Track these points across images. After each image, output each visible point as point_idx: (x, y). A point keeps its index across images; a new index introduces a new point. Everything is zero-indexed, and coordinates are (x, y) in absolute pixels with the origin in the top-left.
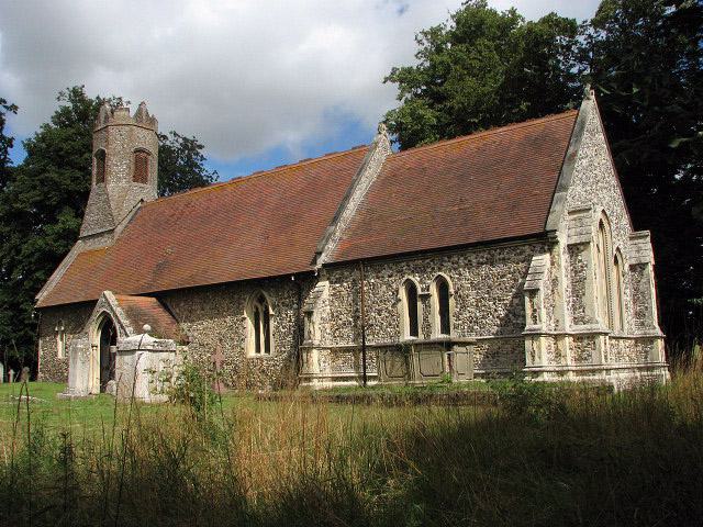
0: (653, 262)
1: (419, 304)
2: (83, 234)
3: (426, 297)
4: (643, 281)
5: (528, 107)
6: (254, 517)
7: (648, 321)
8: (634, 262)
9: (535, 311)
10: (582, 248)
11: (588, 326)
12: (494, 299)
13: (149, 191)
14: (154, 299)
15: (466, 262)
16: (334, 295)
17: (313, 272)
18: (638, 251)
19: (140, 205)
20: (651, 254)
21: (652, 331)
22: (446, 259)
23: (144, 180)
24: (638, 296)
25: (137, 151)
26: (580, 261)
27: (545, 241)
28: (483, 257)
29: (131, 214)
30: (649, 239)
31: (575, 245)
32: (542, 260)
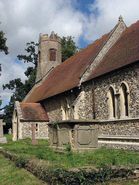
3: (118, 95)
15: (134, 73)
22: (126, 73)
23: (54, 60)
25: (50, 50)
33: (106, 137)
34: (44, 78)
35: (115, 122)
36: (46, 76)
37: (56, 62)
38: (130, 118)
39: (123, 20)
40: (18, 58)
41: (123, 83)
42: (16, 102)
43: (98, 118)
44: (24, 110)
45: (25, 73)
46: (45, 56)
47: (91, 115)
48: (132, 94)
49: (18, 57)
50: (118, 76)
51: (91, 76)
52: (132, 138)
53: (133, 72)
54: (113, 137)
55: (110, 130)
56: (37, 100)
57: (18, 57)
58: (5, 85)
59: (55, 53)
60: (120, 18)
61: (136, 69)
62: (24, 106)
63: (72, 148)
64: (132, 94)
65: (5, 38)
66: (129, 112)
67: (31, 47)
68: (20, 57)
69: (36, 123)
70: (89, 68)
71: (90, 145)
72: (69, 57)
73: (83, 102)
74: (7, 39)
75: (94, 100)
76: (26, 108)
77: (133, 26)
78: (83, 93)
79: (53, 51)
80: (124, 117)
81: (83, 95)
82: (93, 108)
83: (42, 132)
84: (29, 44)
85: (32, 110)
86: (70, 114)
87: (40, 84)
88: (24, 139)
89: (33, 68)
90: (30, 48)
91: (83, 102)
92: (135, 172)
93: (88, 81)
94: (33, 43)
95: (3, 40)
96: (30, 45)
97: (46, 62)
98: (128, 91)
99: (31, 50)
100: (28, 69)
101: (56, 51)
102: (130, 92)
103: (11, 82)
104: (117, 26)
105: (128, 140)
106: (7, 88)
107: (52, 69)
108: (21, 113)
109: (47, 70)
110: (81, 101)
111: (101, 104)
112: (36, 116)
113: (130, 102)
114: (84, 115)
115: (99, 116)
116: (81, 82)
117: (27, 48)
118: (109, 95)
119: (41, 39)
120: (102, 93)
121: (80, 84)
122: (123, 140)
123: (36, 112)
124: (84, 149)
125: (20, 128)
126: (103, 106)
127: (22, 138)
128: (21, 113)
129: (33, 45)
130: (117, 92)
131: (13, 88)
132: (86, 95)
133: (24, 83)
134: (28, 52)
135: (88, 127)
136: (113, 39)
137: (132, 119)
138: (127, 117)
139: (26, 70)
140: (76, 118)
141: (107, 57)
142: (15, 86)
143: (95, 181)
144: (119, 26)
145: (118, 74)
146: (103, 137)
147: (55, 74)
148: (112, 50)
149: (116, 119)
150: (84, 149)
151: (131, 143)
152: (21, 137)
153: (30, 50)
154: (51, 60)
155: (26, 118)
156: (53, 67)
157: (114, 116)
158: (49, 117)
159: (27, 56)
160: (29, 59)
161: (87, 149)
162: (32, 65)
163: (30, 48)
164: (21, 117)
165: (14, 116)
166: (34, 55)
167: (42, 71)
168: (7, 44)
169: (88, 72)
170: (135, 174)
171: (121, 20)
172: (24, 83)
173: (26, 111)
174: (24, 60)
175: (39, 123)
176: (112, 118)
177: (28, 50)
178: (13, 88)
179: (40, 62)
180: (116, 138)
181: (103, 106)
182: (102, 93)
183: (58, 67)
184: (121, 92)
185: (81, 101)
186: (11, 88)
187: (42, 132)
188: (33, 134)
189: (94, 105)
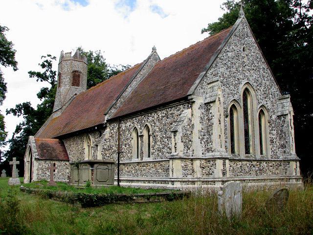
0: (292, 114)
1: (139, 138)
2: (54, 110)
3: (142, 136)
4: (285, 125)
5: (291, 22)
6: (236, 223)
7: (287, 150)
8: (279, 114)
9: (176, 144)
10: (212, 105)
11: (213, 154)
12: (168, 137)
13: (82, 88)
14: (58, 140)
15: (157, 116)
16: (111, 136)
17: (103, 124)
18: (283, 108)
19: (75, 96)
20: (291, 109)
21: (289, 157)
22: (150, 115)
23: (78, 85)
24: (282, 135)
25: (73, 72)
26: (211, 113)
27: (186, 101)
28: (163, 113)
29: (70, 101)
30: (289, 100)
31: (208, 103)
32: (187, 112)
33: (129, 179)
34: (64, 107)
35: (138, 163)
36: (67, 105)
37: (80, 88)
38: (151, 159)
39: (157, 51)
40: (29, 74)
41: (146, 125)
42: (30, 136)
43: (122, 159)
44: (39, 148)
45: (37, 95)
46: (67, 80)
47: (115, 156)
48: (154, 136)
49: (29, 73)
50: (143, 116)
51: (117, 113)
52: (153, 179)
53: (156, 114)
54: (136, 179)
55: (133, 172)
56: (56, 135)
57: (29, 73)
58: (9, 110)
59: (79, 76)
60: (153, 49)
61: (158, 112)
62: (40, 143)
63: (91, 185)
64: (154, 136)
65: (14, 50)
66: (151, 154)
67: (47, 61)
68: (32, 74)
69: (54, 162)
70: (115, 104)
71: (107, 183)
72: (50, 198)
73: (108, 140)
74: (13, 43)
75: (119, 139)
76: (42, 144)
77: (166, 59)
78: (108, 130)
79: (77, 73)
80: (146, 159)
81: (107, 132)
82: (119, 149)
83: (61, 174)
84: (45, 57)
85: (49, 147)
86: (94, 153)
87: (59, 114)
88: (38, 181)
89: (48, 88)
90: (45, 63)
91: (108, 140)
92: (134, 198)
93: (113, 118)
94: (49, 56)
95: (12, 52)
96: (45, 59)
97: (68, 87)
98: (151, 133)
99: (47, 65)
100: (42, 91)
101: (81, 74)
102: (153, 134)
103: (17, 106)
104: (149, 58)
105: (149, 181)
106: (12, 114)
107: (75, 96)
108: (36, 150)
109: (68, 97)
110: (105, 140)
111: (126, 144)
112: (54, 154)
113: (152, 144)
114: (108, 155)
115: (123, 157)
116: (106, 119)
117: (41, 63)
118: (134, 135)
119: (62, 57)
120: (127, 133)
121: (106, 122)
122: (144, 181)
123: (54, 150)
124: (102, 185)
125: (35, 169)
126: (127, 146)
127: (37, 180)
128: (36, 150)
129: (49, 59)
130: (141, 133)
131: (19, 114)
132: (111, 133)
133: (36, 109)
134: (43, 68)
135: (105, 167)
136: (145, 72)
137: (153, 160)
138: (149, 158)
139: (39, 91)
140: (100, 158)
141: (135, 92)
142: (23, 111)
143: (105, 202)
144: (152, 57)
145: (142, 115)
146: (126, 179)
147: (76, 103)
148: (142, 84)
149: (139, 160)
150: (102, 185)
151: (151, 185)
152: (35, 178)
153: (83, 202)
154: (73, 85)
155: (42, 156)
156: (76, 94)
157: (138, 158)
158: (69, 156)
159: (41, 73)
160: (42, 77)
161: (104, 185)
162: (47, 85)
163: (45, 63)
164: (35, 155)
165: (27, 153)
166: (51, 71)
167: (62, 98)
168: (17, 58)
169: (115, 108)
170: (134, 200)
171: (154, 51)
172: (36, 109)
173: (42, 147)
174: (36, 78)
175: (57, 163)
176: (135, 160)
177: (43, 66)
178: (19, 114)
179: (59, 86)
180: (138, 179)
181: (127, 146)
182: (127, 133)
183: (82, 94)
184: (145, 133)
185: (105, 140)
186: (17, 114)
187: (61, 174)
188: (52, 175)
189: (119, 144)
